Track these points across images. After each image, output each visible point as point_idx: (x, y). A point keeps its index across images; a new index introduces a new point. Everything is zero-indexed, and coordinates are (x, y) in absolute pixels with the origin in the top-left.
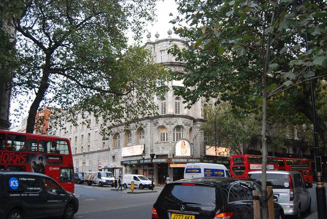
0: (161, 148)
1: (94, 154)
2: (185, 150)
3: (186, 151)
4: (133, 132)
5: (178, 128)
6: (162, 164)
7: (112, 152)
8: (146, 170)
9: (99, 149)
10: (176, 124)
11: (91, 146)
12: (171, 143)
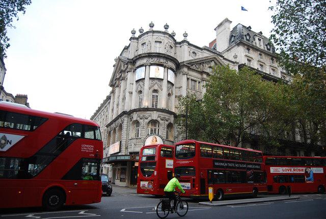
5: (154, 122)
10: (150, 119)
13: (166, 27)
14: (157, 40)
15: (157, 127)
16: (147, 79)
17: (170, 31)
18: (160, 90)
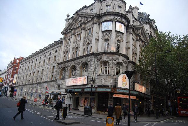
0: (103, 80)
1: (45, 84)
2: (125, 82)
3: (126, 84)
4: (68, 69)
5: (119, 64)
6: (106, 93)
7: (58, 83)
8: (88, 98)
9: (48, 80)
10: (117, 61)
11: (43, 78)
12: (112, 76)
14: (107, 4)
15: (120, 68)
16: (113, 31)
18: (109, 38)
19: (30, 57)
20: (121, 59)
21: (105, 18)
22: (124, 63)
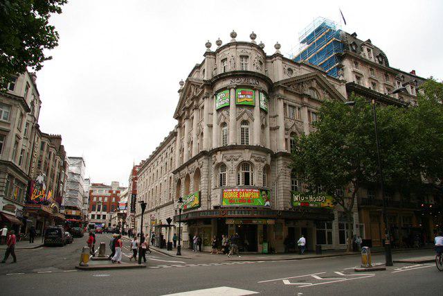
10: (240, 159)
13: (253, 36)
14: (242, 54)
17: (243, 37)
18: (250, 120)
19: (152, 157)
20: (246, 156)
21: (219, 86)
22: (256, 161)
